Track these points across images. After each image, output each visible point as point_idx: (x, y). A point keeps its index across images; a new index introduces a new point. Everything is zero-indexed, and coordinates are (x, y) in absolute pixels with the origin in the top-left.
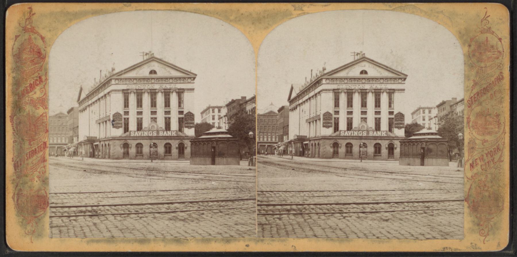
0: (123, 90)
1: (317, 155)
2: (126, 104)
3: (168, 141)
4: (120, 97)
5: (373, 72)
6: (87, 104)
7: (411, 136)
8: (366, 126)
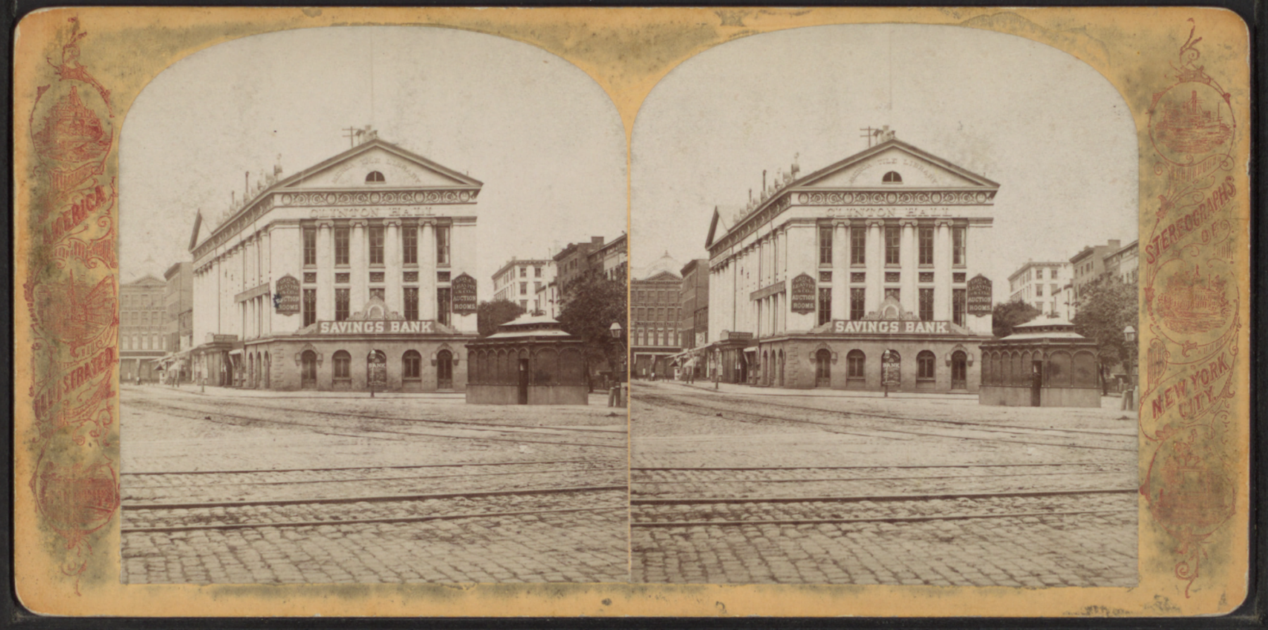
0: (302, 221)
1: (777, 381)
2: (310, 256)
3: (411, 346)
4: (292, 239)
5: (914, 176)
6: (213, 255)
7: (1008, 334)
8: (897, 310)
